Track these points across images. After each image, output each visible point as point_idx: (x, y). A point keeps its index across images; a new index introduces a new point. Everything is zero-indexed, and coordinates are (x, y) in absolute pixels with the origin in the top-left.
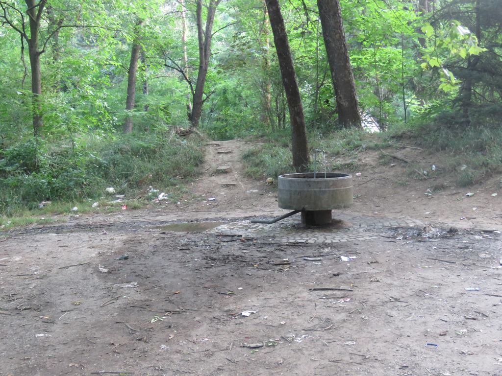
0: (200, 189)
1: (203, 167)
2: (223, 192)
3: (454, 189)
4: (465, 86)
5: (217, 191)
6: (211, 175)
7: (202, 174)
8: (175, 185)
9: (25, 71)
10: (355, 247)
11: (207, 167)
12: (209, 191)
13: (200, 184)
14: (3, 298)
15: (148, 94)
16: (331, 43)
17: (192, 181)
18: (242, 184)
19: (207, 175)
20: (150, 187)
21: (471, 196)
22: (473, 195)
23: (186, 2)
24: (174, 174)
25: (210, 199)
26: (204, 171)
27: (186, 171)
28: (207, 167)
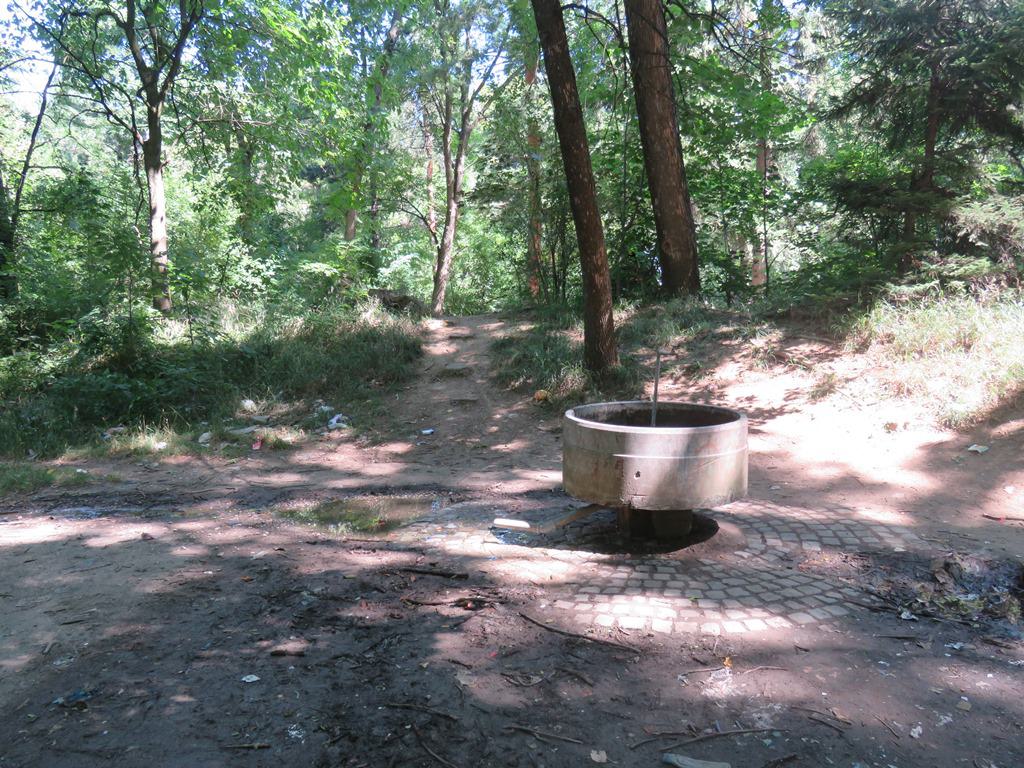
0: (411, 406)
1: (420, 363)
2: (452, 416)
3: (325, 116)
4: (867, 85)
5: (440, 412)
6: (433, 381)
7: (417, 377)
8: (367, 398)
9: (769, 525)
10: (90, 177)
11: (428, 364)
12: (426, 413)
13: (412, 398)
14: (195, 711)
15: (642, 351)
16: (1016, 116)
17: (397, 391)
18: (488, 400)
19: (427, 379)
20: (320, 401)
21: (982, 454)
22: (986, 451)
23: (763, 4)
24: (368, 376)
25: (424, 432)
26: (421, 371)
27: (388, 372)
28: (428, 364)
